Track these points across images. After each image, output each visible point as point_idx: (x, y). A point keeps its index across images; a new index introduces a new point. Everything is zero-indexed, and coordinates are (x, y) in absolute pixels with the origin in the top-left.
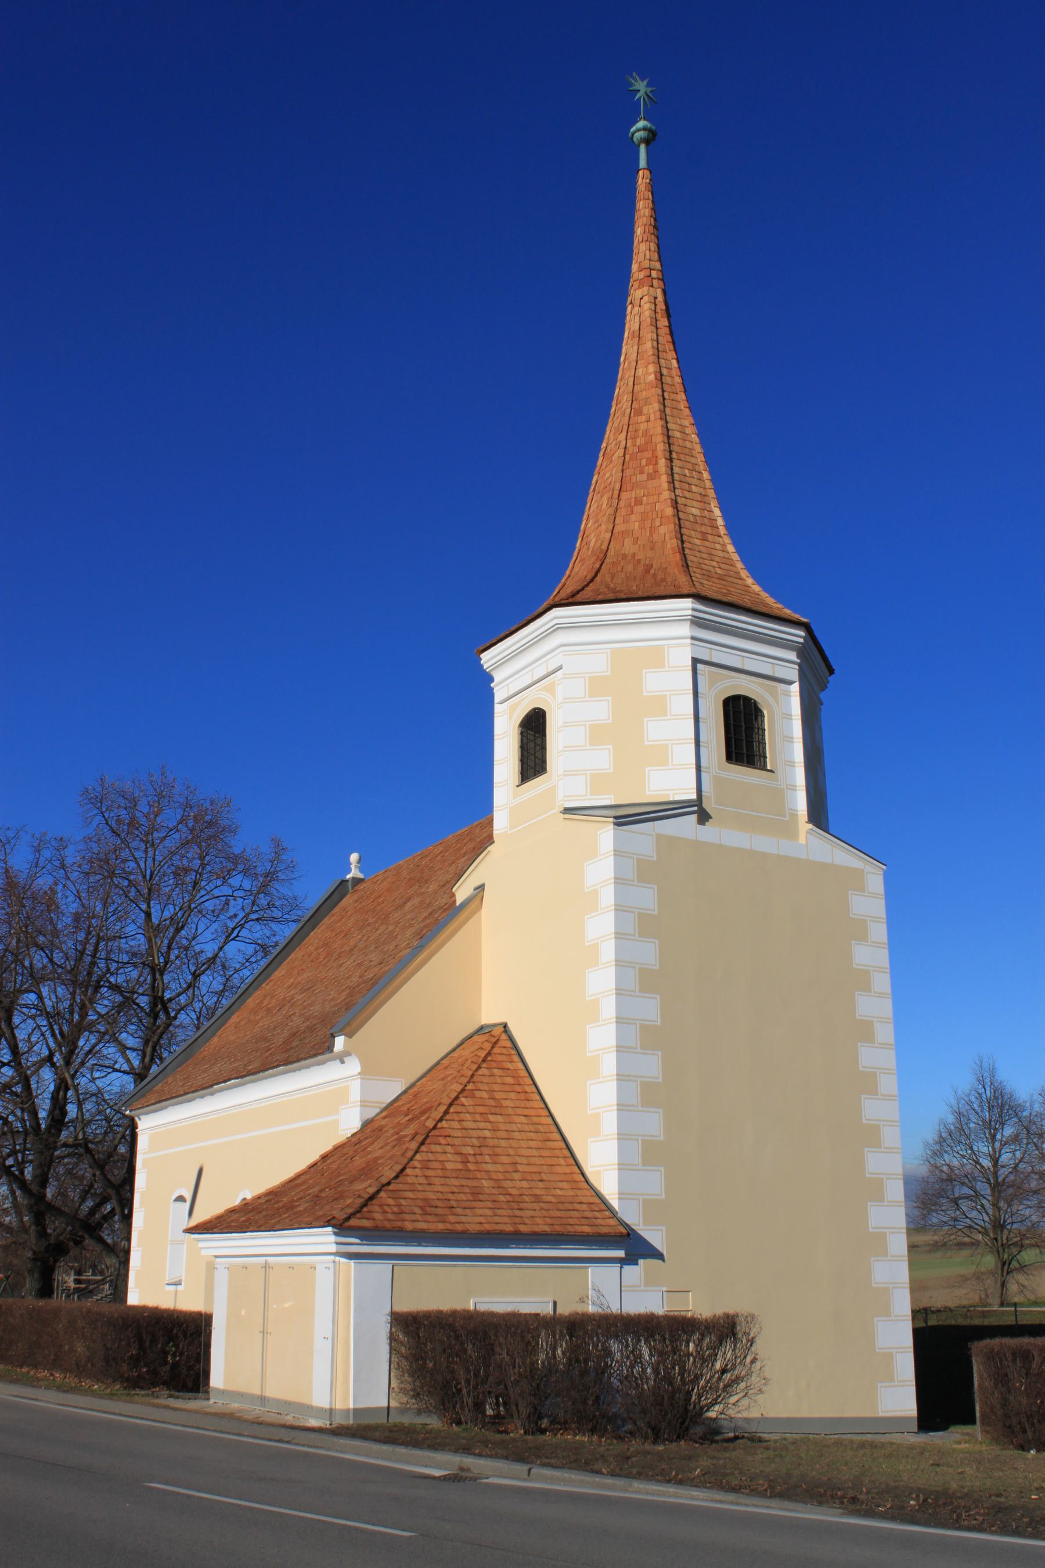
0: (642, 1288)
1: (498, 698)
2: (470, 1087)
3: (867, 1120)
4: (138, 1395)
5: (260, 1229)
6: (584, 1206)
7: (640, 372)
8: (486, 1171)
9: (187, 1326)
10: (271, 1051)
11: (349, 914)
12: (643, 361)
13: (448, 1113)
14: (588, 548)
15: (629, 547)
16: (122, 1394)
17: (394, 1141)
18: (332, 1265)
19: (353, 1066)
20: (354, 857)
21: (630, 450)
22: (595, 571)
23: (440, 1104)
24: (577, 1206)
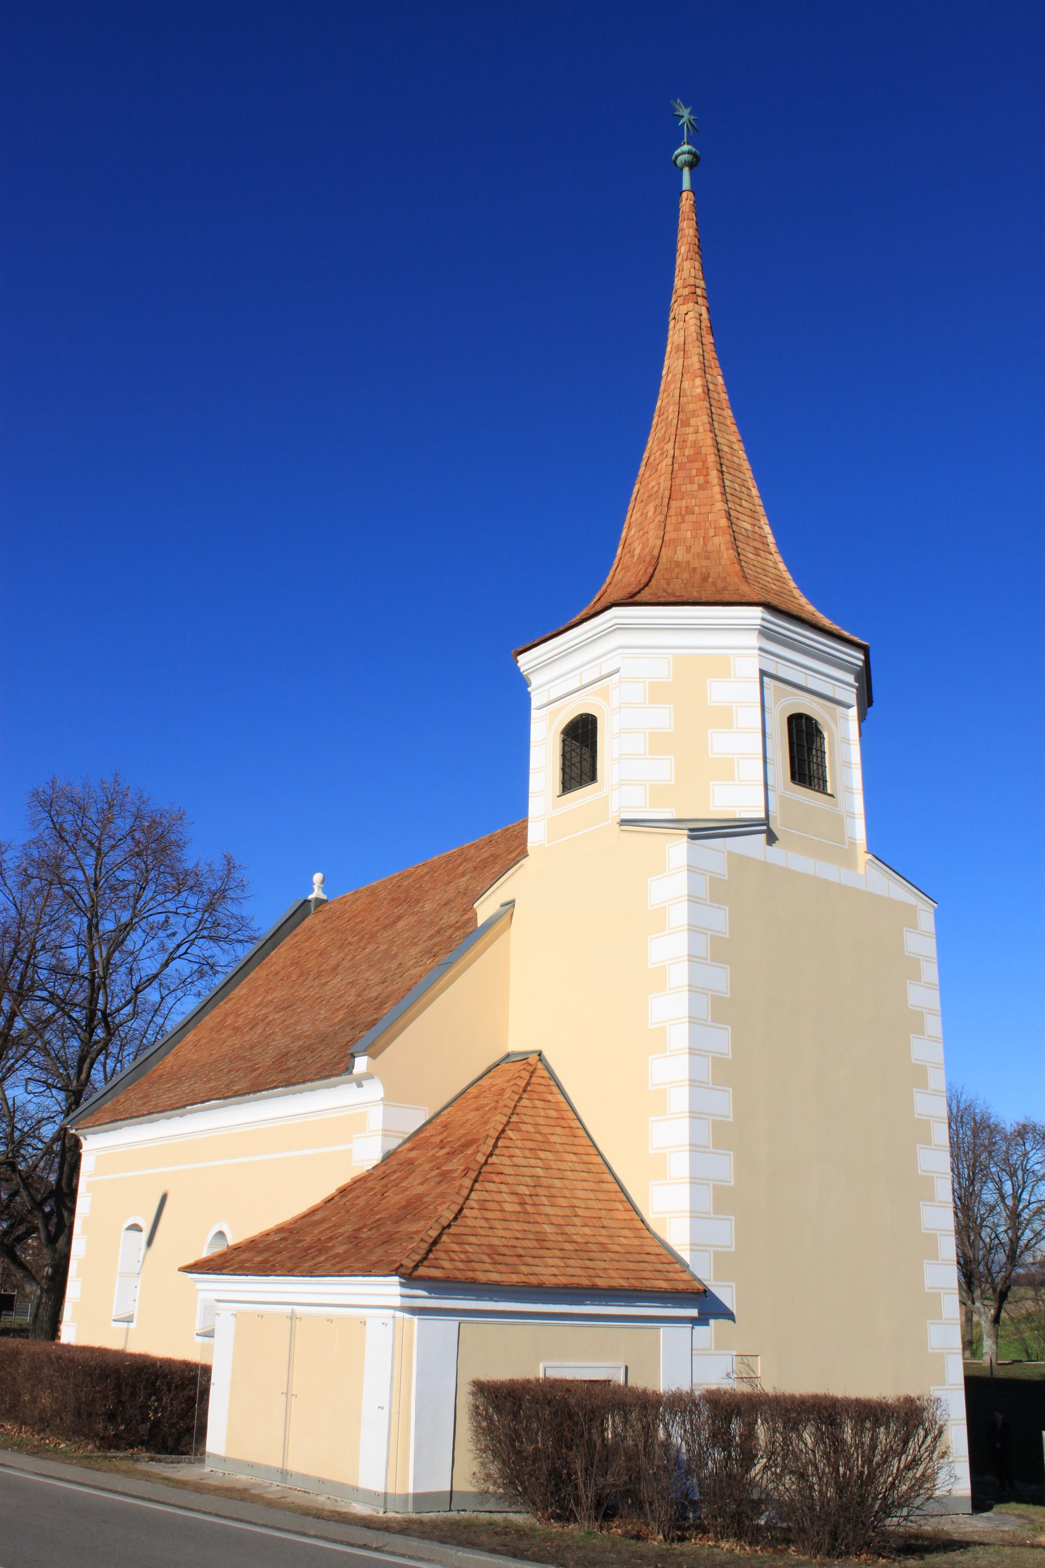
0: (713, 1352)
1: (535, 702)
2: (514, 1119)
3: (923, 1171)
4: (115, 1457)
5: (291, 1273)
6: (653, 1257)
7: (686, 384)
8: (545, 1215)
9: (171, 1378)
10: (258, 1072)
11: (317, 934)
12: (689, 375)
13: (497, 1147)
14: (633, 556)
15: (681, 555)
16: (99, 1457)
17: (435, 1176)
18: (390, 1322)
19: (374, 1090)
20: (318, 877)
21: (679, 459)
22: (649, 575)
23: (488, 1136)
24: (646, 1258)
